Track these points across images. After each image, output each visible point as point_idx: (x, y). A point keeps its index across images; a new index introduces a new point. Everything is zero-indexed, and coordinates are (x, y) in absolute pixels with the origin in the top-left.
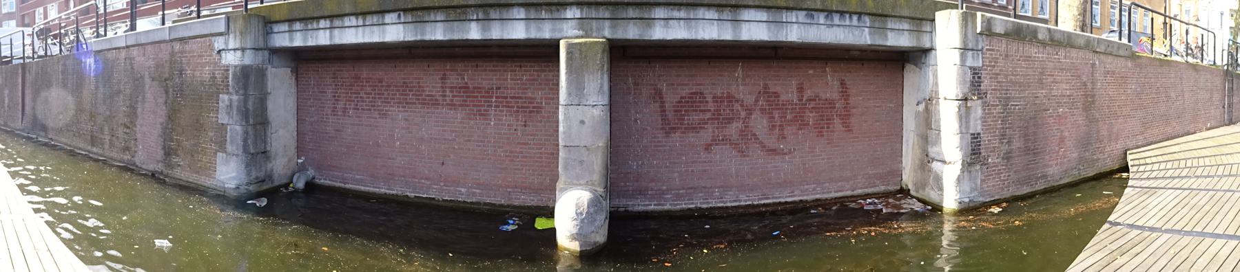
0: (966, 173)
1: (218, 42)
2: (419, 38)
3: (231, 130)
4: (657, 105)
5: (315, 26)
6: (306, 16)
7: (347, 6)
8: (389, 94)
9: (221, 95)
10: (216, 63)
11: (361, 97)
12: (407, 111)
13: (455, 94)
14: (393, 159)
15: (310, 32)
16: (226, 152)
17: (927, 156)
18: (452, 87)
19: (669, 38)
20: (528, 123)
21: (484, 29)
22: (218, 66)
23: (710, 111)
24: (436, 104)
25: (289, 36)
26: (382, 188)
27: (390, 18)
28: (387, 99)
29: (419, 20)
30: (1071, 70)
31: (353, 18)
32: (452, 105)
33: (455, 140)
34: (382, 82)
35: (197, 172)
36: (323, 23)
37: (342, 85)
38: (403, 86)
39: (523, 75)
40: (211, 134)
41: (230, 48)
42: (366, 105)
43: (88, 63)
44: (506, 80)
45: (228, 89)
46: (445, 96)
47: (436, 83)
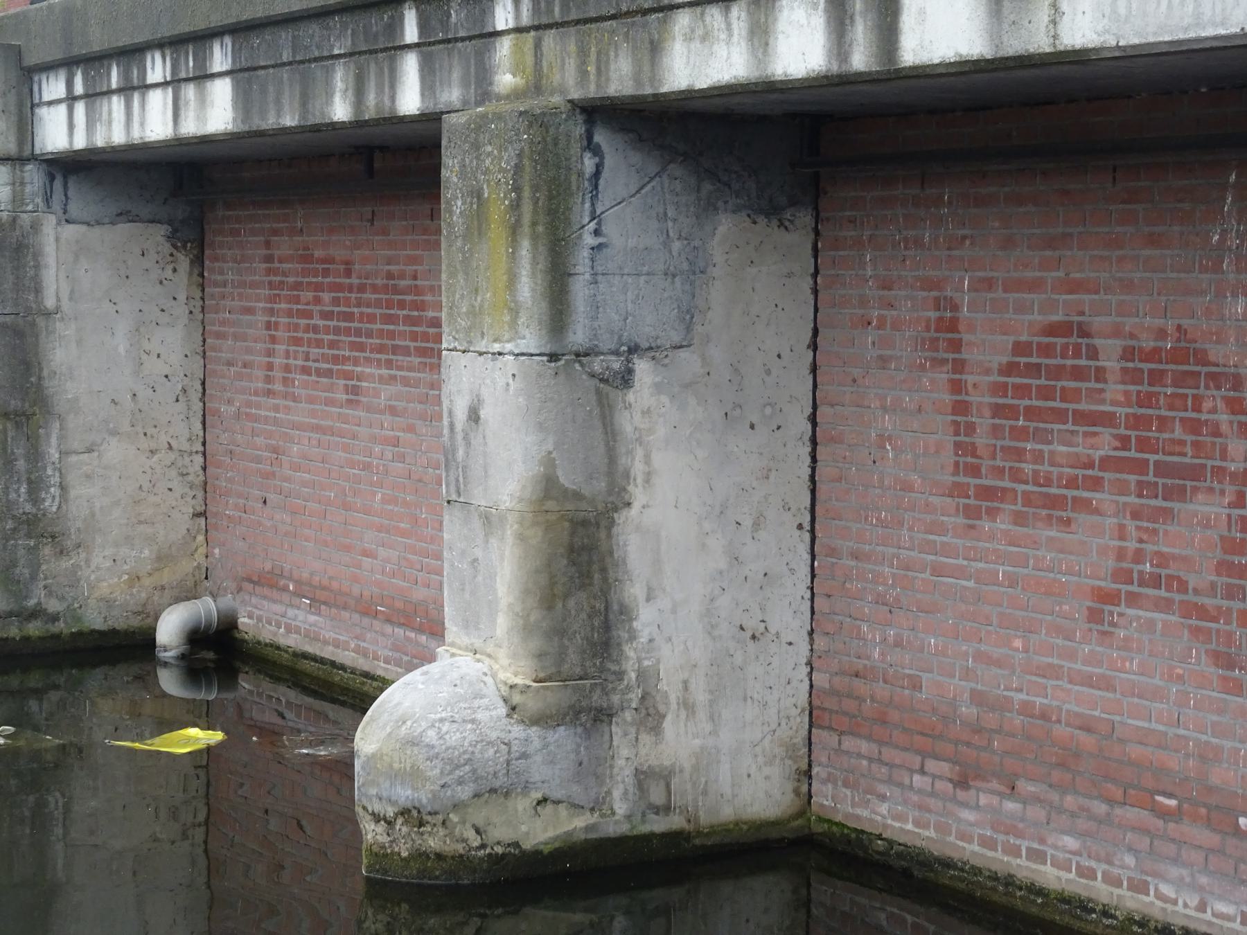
4: (943, 376)
17: (191, 312)
19: (702, 83)
23: (1107, 419)
43: (1002, 506)
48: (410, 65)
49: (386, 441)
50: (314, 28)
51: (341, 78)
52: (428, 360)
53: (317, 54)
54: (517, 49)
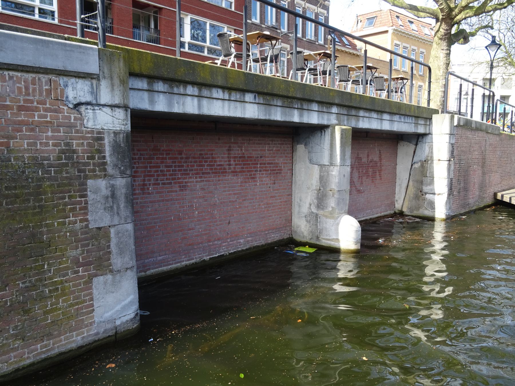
1: (74, 89)
2: (267, 118)
3: (118, 233)
5: (182, 90)
7: (219, 78)
8: (188, 166)
9: (90, 182)
10: (71, 126)
11: (161, 171)
12: (203, 181)
13: (237, 163)
14: (193, 229)
15: (176, 97)
16: (111, 271)
18: (235, 157)
20: (275, 182)
21: (301, 116)
22: (77, 132)
24: (224, 172)
25: (149, 97)
26: (183, 261)
27: (249, 97)
28: (186, 170)
29: (267, 103)
30: (473, 151)
31: (220, 91)
32: (235, 173)
33: (236, 201)
34: (181, 154)
35: (49, 336)
36: (190, 90)
37: (140, 159)
38: (199, 158)
39: (273, 148)
40: (73, 253)
41: (102, 102)
42: (167, 179)
44: (265, 150)
45: (105, 170)
46: (230, 165)
47: (224, 154)
49: (200, 197)
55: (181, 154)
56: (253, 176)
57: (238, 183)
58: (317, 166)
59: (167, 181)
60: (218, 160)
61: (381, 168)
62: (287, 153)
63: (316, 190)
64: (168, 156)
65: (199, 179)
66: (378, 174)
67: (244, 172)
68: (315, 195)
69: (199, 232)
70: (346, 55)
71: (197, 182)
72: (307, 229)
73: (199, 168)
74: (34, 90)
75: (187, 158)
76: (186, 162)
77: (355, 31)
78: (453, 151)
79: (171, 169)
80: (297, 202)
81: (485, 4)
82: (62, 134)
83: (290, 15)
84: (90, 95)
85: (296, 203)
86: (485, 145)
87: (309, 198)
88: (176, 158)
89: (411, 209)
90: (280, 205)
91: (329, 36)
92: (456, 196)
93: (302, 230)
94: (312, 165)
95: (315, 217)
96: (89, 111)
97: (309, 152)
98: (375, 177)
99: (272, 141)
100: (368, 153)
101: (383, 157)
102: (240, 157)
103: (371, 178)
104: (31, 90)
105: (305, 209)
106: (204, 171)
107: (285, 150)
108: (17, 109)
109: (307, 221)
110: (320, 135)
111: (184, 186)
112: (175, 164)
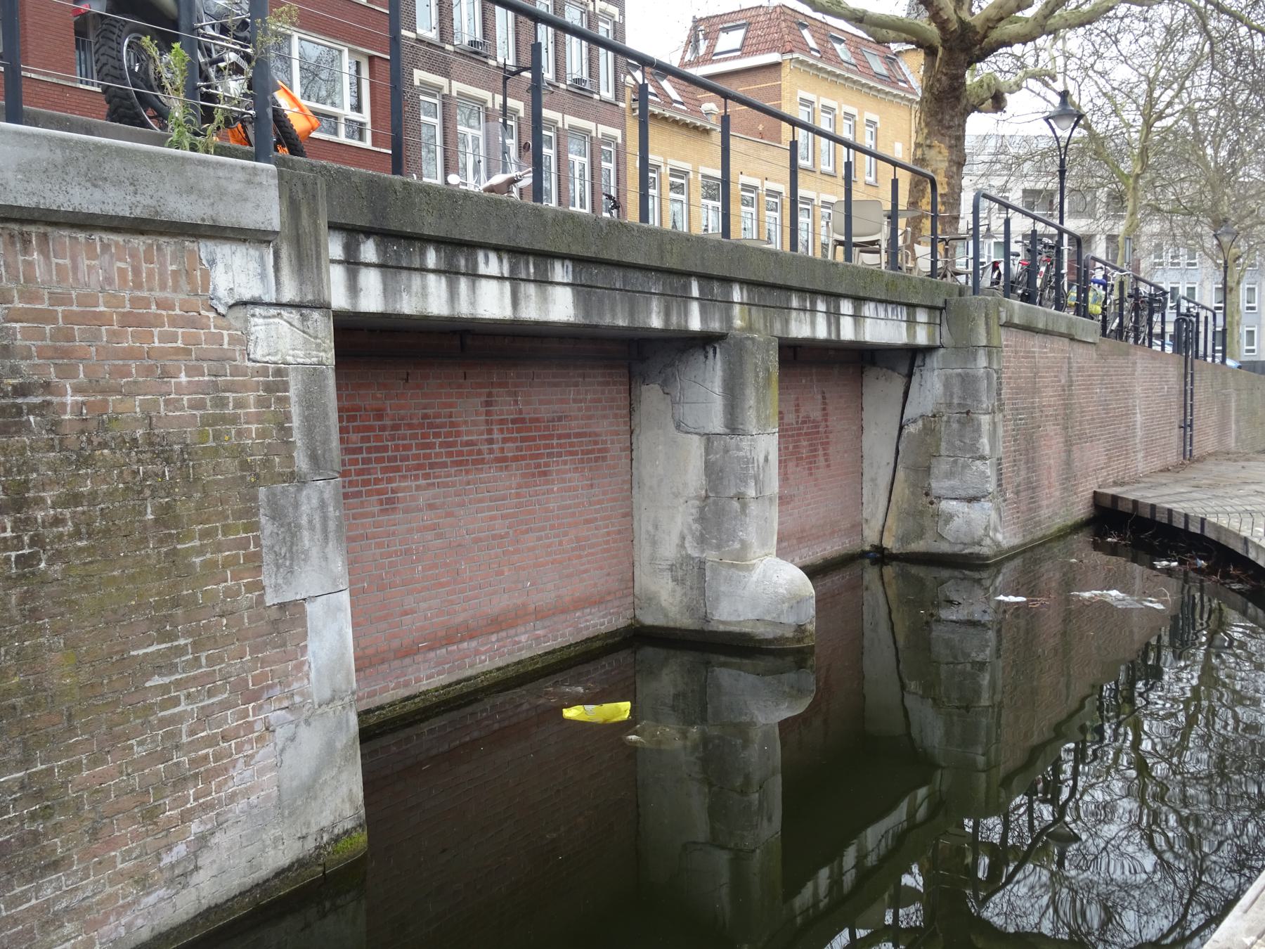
0: (791, 464)
1: (228, 268)
6: (456, 235)
10: (223, 358)
14: (412, 612)
18: (502, 422)
28: (394, 459)
34: (380, 417)
38: (421, 426)
39: (586, 394)
47: (477, 414)
48: (695, 308)
49: (426, 528)
50: (638, 274)
51: (655, 305)
52: (463, 468)
53: (640, 289)
54: (742, 311)
55: (380, 417)
56: (543, 469)
57: (511, 488)
58: (696, 438)
59: (351, 490)
60: (463, 428)
61: (827, 437)
62: (619, 408)
63: (698, 497)
64: (351, 424)
65: (422, 482)
66: (821, 452)
67: (523, 458)
68: (694, 511)
69: (426, 618)
70: (676, 129)
71: (418, 488)
72: (678, 599)
73: (422, 452)
74: (150, 274)
75: (396, 427)
76: (393, 438)
77: (690, 64)
78: (1000, 389)
79: (360, 456)
80: (648, 532)
81: (1048, 12)
82: (206, 378)
83: (521, 18)
84: (259, 281)
85: (644, 536)
86: (1069, 372)
87: (679, 520)
88: (370, 429)
89: (904, 539)
90: (607, 542)
91: (629, 78)
92: (1010, 504)
93: (664, 604)
94: (684, 435)
95: (696, 569)
96: (256, 319)
97: (673, 403)
98: (815, 462)
99: (584, 377)
100: (797, 399)
101: (830, 408)
102: (514, 421)
103: (807, 463)
104: (144, 275)
105: (669, 551)
106: (433, 460)
107: (613, 400)
108: (119, 322)
109: (675, 580)
110: (702, 358)
111: (390, 501)
112: (368, 445)
